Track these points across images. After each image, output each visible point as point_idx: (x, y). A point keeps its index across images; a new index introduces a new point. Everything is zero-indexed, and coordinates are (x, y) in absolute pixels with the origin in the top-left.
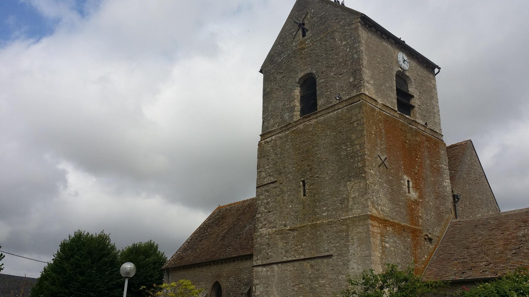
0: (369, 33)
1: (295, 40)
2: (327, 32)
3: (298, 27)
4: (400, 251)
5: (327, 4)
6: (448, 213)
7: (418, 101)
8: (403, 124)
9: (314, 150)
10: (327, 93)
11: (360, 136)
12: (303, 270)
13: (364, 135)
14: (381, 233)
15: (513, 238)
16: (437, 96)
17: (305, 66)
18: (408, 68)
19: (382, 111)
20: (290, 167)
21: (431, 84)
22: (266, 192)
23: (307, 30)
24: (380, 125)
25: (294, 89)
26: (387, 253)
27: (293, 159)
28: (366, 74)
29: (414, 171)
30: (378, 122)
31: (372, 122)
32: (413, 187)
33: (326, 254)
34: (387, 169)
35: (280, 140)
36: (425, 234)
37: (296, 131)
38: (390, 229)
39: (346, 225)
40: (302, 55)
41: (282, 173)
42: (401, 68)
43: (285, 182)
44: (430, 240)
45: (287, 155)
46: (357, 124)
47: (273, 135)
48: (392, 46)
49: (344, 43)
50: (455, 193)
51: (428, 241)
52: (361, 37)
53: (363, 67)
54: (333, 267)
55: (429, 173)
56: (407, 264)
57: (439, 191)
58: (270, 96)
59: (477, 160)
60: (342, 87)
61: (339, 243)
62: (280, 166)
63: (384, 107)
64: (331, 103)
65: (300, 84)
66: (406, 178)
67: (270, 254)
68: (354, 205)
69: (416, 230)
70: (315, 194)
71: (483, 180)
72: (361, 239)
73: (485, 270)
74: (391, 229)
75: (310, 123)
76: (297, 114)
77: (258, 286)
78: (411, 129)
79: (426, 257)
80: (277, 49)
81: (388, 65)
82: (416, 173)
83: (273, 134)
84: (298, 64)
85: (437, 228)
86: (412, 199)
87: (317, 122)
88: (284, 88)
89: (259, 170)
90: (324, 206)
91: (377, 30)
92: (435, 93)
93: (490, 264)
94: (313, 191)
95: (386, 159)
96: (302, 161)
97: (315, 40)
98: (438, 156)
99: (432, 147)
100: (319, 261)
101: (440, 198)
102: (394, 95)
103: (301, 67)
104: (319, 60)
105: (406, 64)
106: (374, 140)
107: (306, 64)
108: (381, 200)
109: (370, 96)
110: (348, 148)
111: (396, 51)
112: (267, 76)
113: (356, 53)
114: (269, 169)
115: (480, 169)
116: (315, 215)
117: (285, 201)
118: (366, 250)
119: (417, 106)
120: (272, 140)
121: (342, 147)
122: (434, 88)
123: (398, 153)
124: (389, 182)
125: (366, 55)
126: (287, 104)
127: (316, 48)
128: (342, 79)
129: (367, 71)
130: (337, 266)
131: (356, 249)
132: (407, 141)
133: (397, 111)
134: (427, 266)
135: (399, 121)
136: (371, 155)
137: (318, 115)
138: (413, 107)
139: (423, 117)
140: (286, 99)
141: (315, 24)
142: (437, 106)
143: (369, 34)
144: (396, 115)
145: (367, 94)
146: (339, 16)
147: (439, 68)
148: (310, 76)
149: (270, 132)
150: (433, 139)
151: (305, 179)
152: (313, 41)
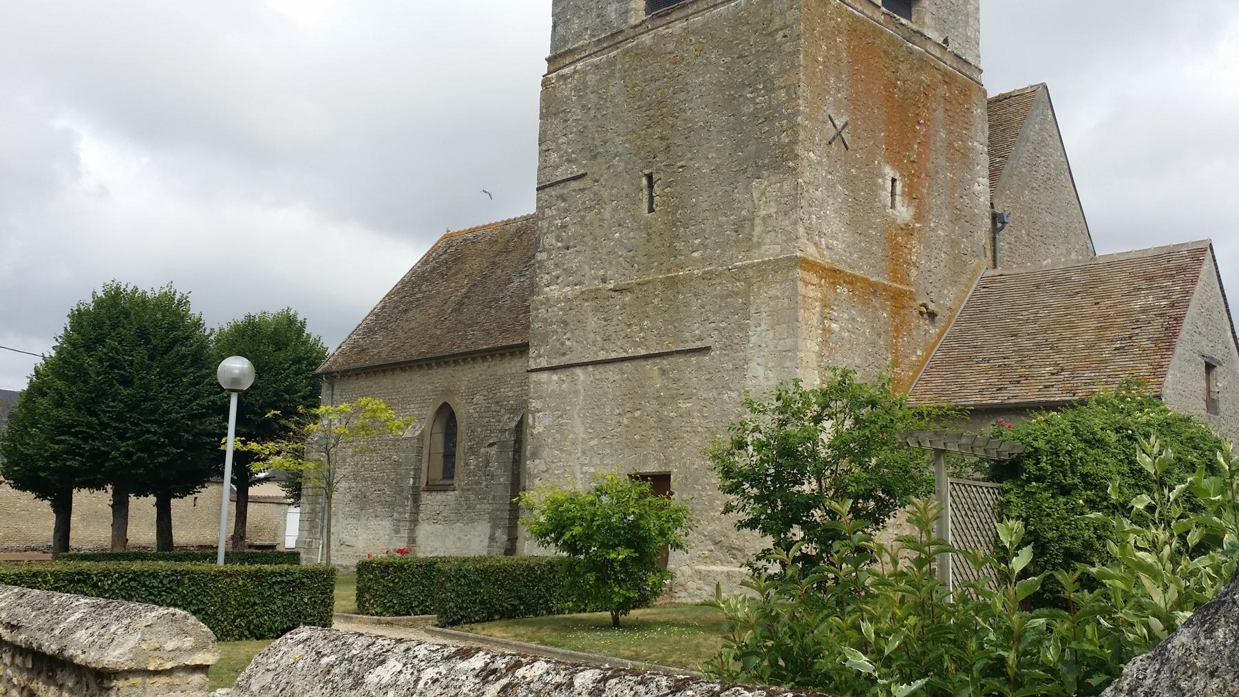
6: (977, 255)
11: (788, 67)
12: (643, 381)
13: (800, 65)
14: (822, 300)
15: (1119, 315)
19: (845, 6)
22: (559, 202)
24: (838, 39)
29: (909, 157)
30: (834, 33)
31: (821, 33)
32: (903, 193)
33: (695, 344)
36: (921, 302)
38: (843, 290)
44: (932, 315)
46: (785, 36)
47: (578, 60)
50: (998, 210)
51: (926, 319)
54: (710, 373)
55: (942, 161)
56: (876, 369)
57: (961, 203)
59: (1055, 132)
61: (728, 320)
62: (593, 139)
66: (889, 172)
67: (568, 343)
68: (764, 235)
69: (902, 294)
74: (846, 290)
75: (670, 31)
77: (540, 414)
78: (911, 52)
79: (919, 353)
82: (913, 162)
83: (577, 57)
86: (899, 221)
87: (686, 29)
89: (544, 147)
90: (696, 236)
93: (1063, 370)
95: (846, 124)
98: (967, 120)
99: (955, 99)
100: (681, 360)
114: (569, 144)
116: (675, 257)
120: (575, 72)
124: (849, 181)
132: (899, 82)
133: (879, 7)
135: (882, 32)
137: (690, 11)
139: (941, 23)
149: (570, 52)
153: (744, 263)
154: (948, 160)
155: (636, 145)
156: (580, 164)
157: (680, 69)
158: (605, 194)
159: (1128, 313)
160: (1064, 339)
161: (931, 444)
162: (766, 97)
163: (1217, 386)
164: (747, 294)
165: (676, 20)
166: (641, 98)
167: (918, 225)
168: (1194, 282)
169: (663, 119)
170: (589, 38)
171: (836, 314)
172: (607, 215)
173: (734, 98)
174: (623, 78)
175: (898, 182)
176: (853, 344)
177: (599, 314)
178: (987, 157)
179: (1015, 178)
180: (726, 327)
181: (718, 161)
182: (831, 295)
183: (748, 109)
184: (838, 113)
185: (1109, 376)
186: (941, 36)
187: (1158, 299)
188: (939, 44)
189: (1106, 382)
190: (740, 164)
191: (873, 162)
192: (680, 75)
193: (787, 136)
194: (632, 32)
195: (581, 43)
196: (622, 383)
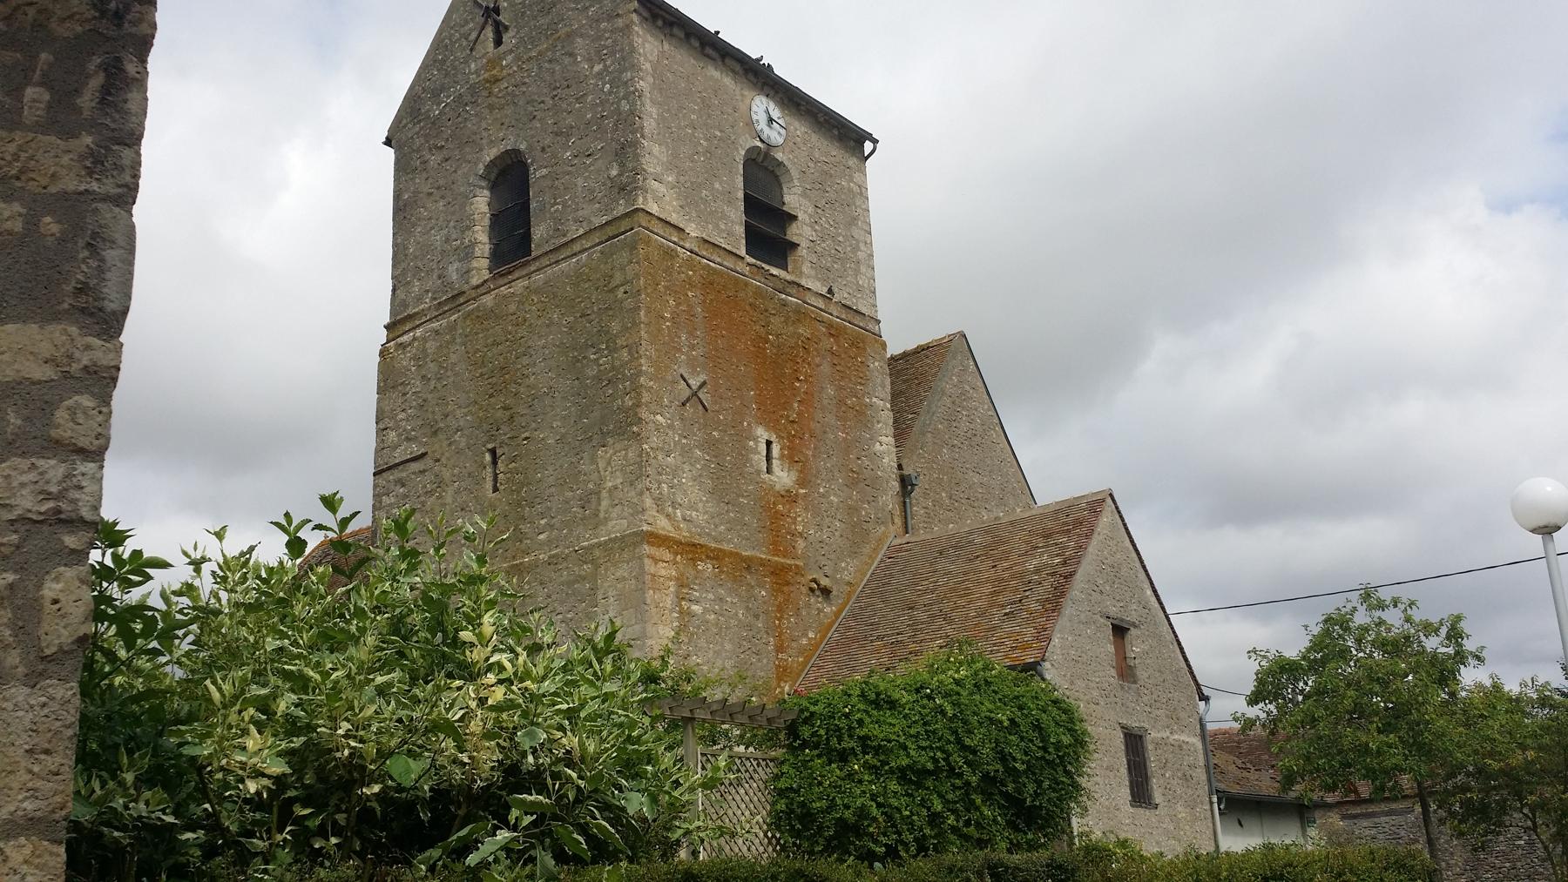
1: (474, 53)
3: (483, 19)
4: (733, 622)
6: (883, 523)
8: (758, 293)
9: (520, 366)
10: (556, 207)
14: (677, 579)
15: (1013, 577)
16: (869, 216)
17: (501, 129)
18: (780, 141)
19: (698, 258)
20: (459, 413)
21: (852, 185)
22: (398, 487)
23: (506, 28)
24: (690, 294)
25: (472, 195)
26: (694, 628)
28: (653, 155)
29: (788, 416)
31: (665, 287)
32: (782, 457)
35: (434, 340)
36: (811, 578)
37: (476, 314)
38: (706, 567)
39: (593, 562)
41: (439, 432)
42: (761, 140)
43: (447, 454)
44: (826, 592)
45: (454, 382)
46: (626, 292)
47: (418, 326)
48: (734, 79)
49: (597, 68)
50: (905, 472)
51: (818, 596)
52: (640, 54)
55: (831, 419)
57: (859, 465)
58: (412, 215)
59: (980, 384)
60: (592, 191)
62: (433, 412)
63: (706, 246)
64: (564, 236)
65: (489, 180)
66: (762, 434)
68: (610, 510)
70: (522, 485)
71: (994, 436)
72: (625, 597)
74: (709, 566)
75: (512, 290)
76: (481, 266)
78: (784, 304)
79: (811, 635)
81: (721, 131)
82: (793, 422)
84: (484, 125)
86: (778, 487)
87: (527, 288)
88: (447, 191)
89: (382, 426)
90: (542, 515)
91: (688, 36)
92: (863, 207)
94: (517, 477)
95: (704, 384)
96: (490, 397)
98: (861, 375)
99: (846, 353)
101: (862, 485)
102: (736, 217)
103: (491, 132)
106: (669, 335)
107: (502, 124)
108: (685, 493)
111: (746, 93)
112: (405, 155)
113: (626, 97)
114: (408, 420)
115: (986, 407)
116: (521, 541)
118: (636, 623)
119: (804, 244)
120: (415, 339)
121: (587, 355)
122: (861, 194)
124: (710, 445)
126: (454, 236)
127: (527, 80)
128: (592, 168)
129: (656, 149)
132: (771, 337)
133: (743, 258)
134: (813, 659)
135: (746, 284)
136: (660, 376)
137: (532, 268)
139: (823, 272)
140: (452, 224)
142: (869, 244)
143: (666, 46)
144: (740, 267)
145: (653, 212)
147: (875, 142)
149: (410, 317)
150: (849, 331)
152: (519, 59)
154: (838, 418)
155: (478, 417)
156: (421, 443)
157: (522, 332)
158: (446, 474)
159: (1022, 575)
160: (957, 608)
161: (671, 712)
162: (609, 357)
165: (518, 279)
168: (1089, 536)
169: (505, 387)
171: (698, 594)
172: (449, 500)
173: (578, 361)
175: (774, 445)
176: (721, 628)
178: (891, 414)
179: (929, 435)
181: (563, 430)
182: (691, 573)
183: (591, 372)
184: (694, 373)
185: (994, 645)
187: (1051, 557)
189: (991, 651)
191: (742, 423)
193: (631, 399)
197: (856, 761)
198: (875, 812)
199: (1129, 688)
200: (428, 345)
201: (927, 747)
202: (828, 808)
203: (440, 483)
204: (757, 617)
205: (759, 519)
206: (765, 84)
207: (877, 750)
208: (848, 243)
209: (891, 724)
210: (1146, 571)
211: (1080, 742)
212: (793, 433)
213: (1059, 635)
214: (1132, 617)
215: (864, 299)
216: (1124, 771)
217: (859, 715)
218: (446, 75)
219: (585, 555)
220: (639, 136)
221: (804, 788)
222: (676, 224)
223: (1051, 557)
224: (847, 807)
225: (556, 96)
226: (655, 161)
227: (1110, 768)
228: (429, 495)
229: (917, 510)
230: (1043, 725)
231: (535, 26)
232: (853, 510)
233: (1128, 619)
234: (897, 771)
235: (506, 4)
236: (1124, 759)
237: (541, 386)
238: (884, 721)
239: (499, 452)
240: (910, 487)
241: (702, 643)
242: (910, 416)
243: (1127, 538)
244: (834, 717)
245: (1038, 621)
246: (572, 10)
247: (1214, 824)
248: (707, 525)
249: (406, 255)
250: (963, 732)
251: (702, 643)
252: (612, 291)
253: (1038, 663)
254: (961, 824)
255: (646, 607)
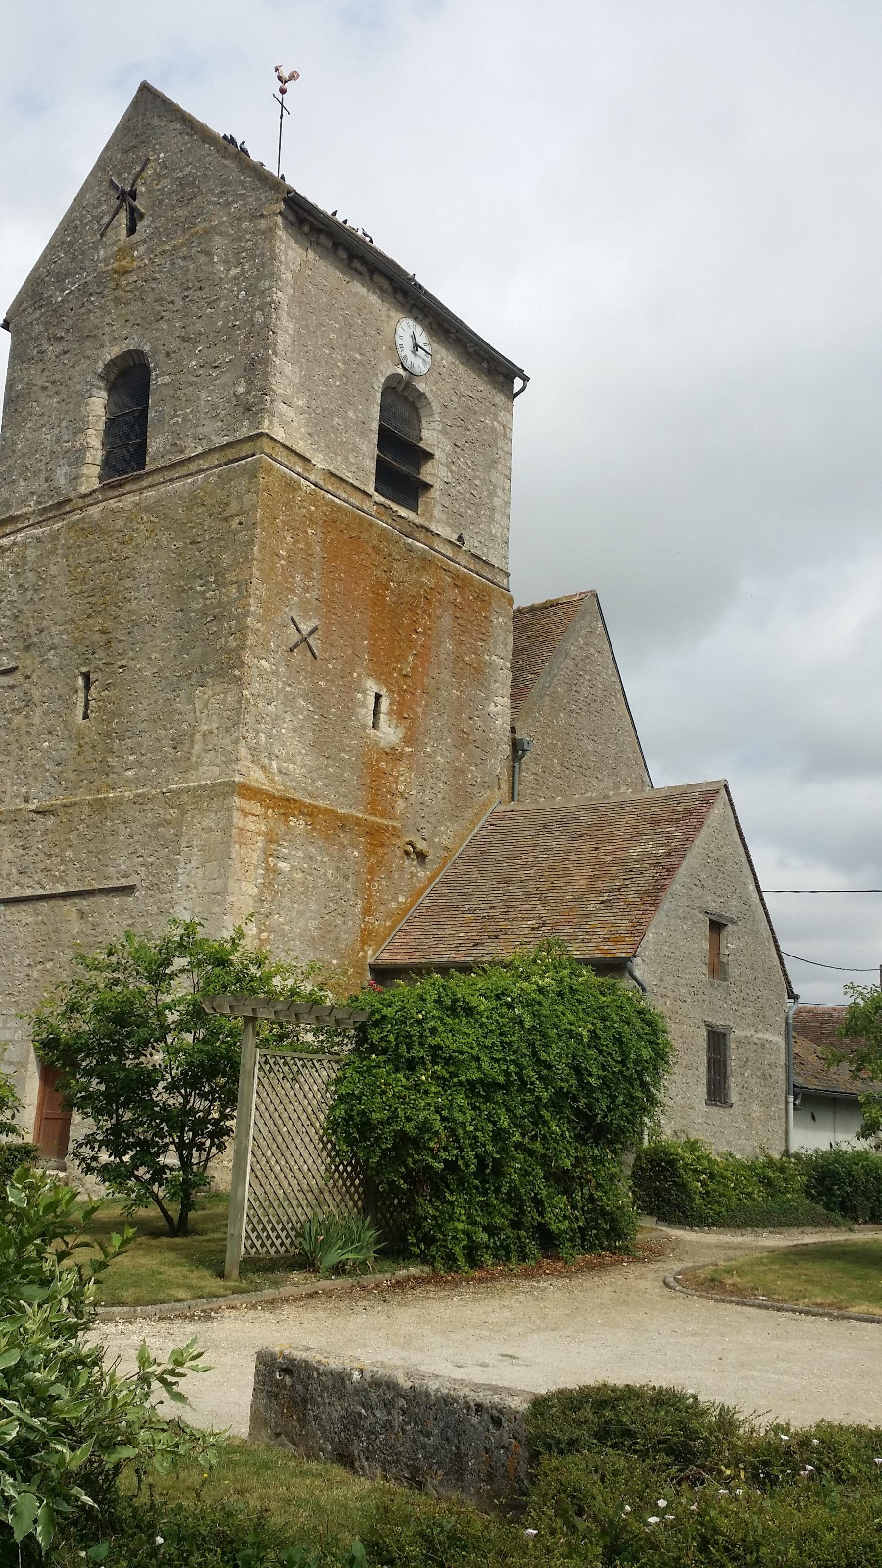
0: (309, 251)
2: (192, 231)
3: (118, 202)
5: (204, 142)
7: (445, 469)
8: (383, 535)
11: (241, 560)
12: (59, 925)
13: (253, 559)
14: (266, 834)
15: (615, 863)
18: (424, 370)
19: (323, 492)
21: (496, 424)
23: (142, 216)
24: (309, 531)
25: (88, 395)
27: (65, 609)
29: (401, 670)
30: (304, 523)
31: (283, 522)
32: (390, 712)
33: (120, 882)
34: (315, 658)
36: (407, 840)
37: (81, 525)
38: (298, 824)
40: (121, 292)
42: (404, 368)
43: (38, 672)
44: (421, 856)
46: (240, 524)
49: (234, 272)
50: (518, 736)
51: (413, 860)
52: (281, 262)
53: (275, 354)
54: (132, 917)
55: (446, 675)
56: (340, 917)
57: (471, 726)
58: (24, 408)
59: (606, 647)
60: (215, 407)
61: (156, 854)
62: (28, 625)
63: (333, 479)
64: (182, 452)
66: (372, 686)
68: (203, 755)
69: (380, 829)
70: (114, 715)
73: (527, 940)
74: (302, 822)
78: (410, 549)
79: (401, 899)
80: (55, 262)
82: (405, 676)
83: (20, 526)
84: (108, 319)
85: (446, 826)
87: (137, 504)
91: (336, 245)
93: (544, 925)
95: (315, 629)
96: (88, 617)
97: (159, 250)
98: (483, 631)
99: (469, 606)
100: (102, 900)
101: (471, 747)
103: (114, 328)
104: (164, 313)
105: (420, 357)
106: (283, 575)
108: (284, 745)
109: (287, 444)
110: (209, 590)
113: (260, 308)
115: (610, 672)
116: (107, 775)
117: (34, 731)
119: (438, 485)
120: (15, 544)
122: (505, 435)
123: (358, 615)
124: (316, 696)
125: (292, 318)
126: (66, 438)
127: (157, 276)
128: (218, 382)
129: (288, 368)
130: (143, 916)
131: (193, 872)
132: (392, 584)
133: (370, 496)
135: (372, 525)
137: (145, 483)
138: (427, 487)
139: (455, 517)
140: (64, 423)
141: (162, 201)
142: (507, 491)
144: (367, 505)
146: (229, 184)
147: (526, 379)
148: (137, 362)
149: (13, 519)
151: (92, 670)
152: (152, 252)
153: (180, 786)
157: (127, 551)
158: (36, 694)
160: (554, 888)
162: (217, 592)
163: (727, 947)
164: (179, 823)
165: (128, 493)
166: (83, 582)
167: (408, 749)
168: (697, 829)
169: (105, 609)
170: (35, 505)
171: (286, 851)
172: (36, 720)
173: (184, 591)
174: (65, 556)
176: (308, 887)
177: (17, 840)
179: (547, 698)
180: (155, 862)
184: (306, 616)
185: (587, 933)
186: (456, 532)
187: (656, 846)
188: (450, 542)
190: (184, 668)
191: (351, 674)
192: (127, 557)
193: (235, 640)
194: (80, 502)
195: (25, 510)
196: (35, 927)
197: (424, 1071)
198: (438, 1126)
199: (719, 986)
200: (28, 552)
201: (501, 1059)
202: (388, 1118)
203: (29, 703)
204: (346, 877)
205: (360, 776)
206: (414, 306)
207: (447, 1061)
208: (484, 488)
209: (465, 1034)
210: (751, 866)
211: (660, 1055)
212: (405, 687)
213: (653, 931)
214: (731, 911)
215: (495, 550)
216: (703, 1069)
217: (432, 1023)
218: (73, 259)
219: (172, 799)
220: (271, 352)
221: (366, 1096)
222: (302, 453)
223: (656, 846)
224: (409, 1119)
225: (187, 297)
226: (286, 382)
227: (689, 1067)
228: (16, 712)
229: (526, 775)
230: (624, 1040)
231: (172, 217)
232: (459, 772)
233: (727, 915)
234: (466, 1084)
235: (143, 189)
236: (705, 1058)
237: (142, 612)
238: (459, 1030)
239: (93, 677)
240: (521, 752)
241: (286, 901)
242: (530, 676)
243: (737, 831)
244: (405, 1023)
245: (634, 913)
246: (214, 203)
247: (787, 1123)
248: (304, 778)
249: (14, 451)
250: (540, 1045)
251: (286, 901)
252: (226, 520)
253: (628, 959)
254: (527, 1140)
255: (230, 862)
